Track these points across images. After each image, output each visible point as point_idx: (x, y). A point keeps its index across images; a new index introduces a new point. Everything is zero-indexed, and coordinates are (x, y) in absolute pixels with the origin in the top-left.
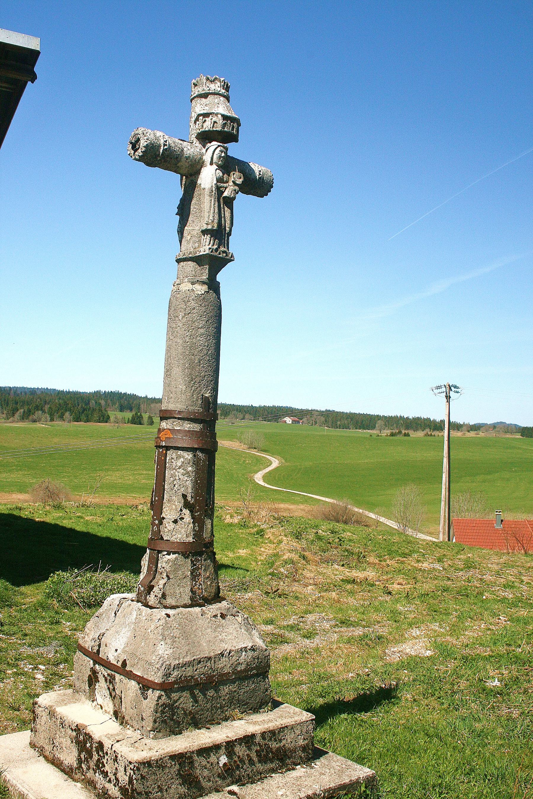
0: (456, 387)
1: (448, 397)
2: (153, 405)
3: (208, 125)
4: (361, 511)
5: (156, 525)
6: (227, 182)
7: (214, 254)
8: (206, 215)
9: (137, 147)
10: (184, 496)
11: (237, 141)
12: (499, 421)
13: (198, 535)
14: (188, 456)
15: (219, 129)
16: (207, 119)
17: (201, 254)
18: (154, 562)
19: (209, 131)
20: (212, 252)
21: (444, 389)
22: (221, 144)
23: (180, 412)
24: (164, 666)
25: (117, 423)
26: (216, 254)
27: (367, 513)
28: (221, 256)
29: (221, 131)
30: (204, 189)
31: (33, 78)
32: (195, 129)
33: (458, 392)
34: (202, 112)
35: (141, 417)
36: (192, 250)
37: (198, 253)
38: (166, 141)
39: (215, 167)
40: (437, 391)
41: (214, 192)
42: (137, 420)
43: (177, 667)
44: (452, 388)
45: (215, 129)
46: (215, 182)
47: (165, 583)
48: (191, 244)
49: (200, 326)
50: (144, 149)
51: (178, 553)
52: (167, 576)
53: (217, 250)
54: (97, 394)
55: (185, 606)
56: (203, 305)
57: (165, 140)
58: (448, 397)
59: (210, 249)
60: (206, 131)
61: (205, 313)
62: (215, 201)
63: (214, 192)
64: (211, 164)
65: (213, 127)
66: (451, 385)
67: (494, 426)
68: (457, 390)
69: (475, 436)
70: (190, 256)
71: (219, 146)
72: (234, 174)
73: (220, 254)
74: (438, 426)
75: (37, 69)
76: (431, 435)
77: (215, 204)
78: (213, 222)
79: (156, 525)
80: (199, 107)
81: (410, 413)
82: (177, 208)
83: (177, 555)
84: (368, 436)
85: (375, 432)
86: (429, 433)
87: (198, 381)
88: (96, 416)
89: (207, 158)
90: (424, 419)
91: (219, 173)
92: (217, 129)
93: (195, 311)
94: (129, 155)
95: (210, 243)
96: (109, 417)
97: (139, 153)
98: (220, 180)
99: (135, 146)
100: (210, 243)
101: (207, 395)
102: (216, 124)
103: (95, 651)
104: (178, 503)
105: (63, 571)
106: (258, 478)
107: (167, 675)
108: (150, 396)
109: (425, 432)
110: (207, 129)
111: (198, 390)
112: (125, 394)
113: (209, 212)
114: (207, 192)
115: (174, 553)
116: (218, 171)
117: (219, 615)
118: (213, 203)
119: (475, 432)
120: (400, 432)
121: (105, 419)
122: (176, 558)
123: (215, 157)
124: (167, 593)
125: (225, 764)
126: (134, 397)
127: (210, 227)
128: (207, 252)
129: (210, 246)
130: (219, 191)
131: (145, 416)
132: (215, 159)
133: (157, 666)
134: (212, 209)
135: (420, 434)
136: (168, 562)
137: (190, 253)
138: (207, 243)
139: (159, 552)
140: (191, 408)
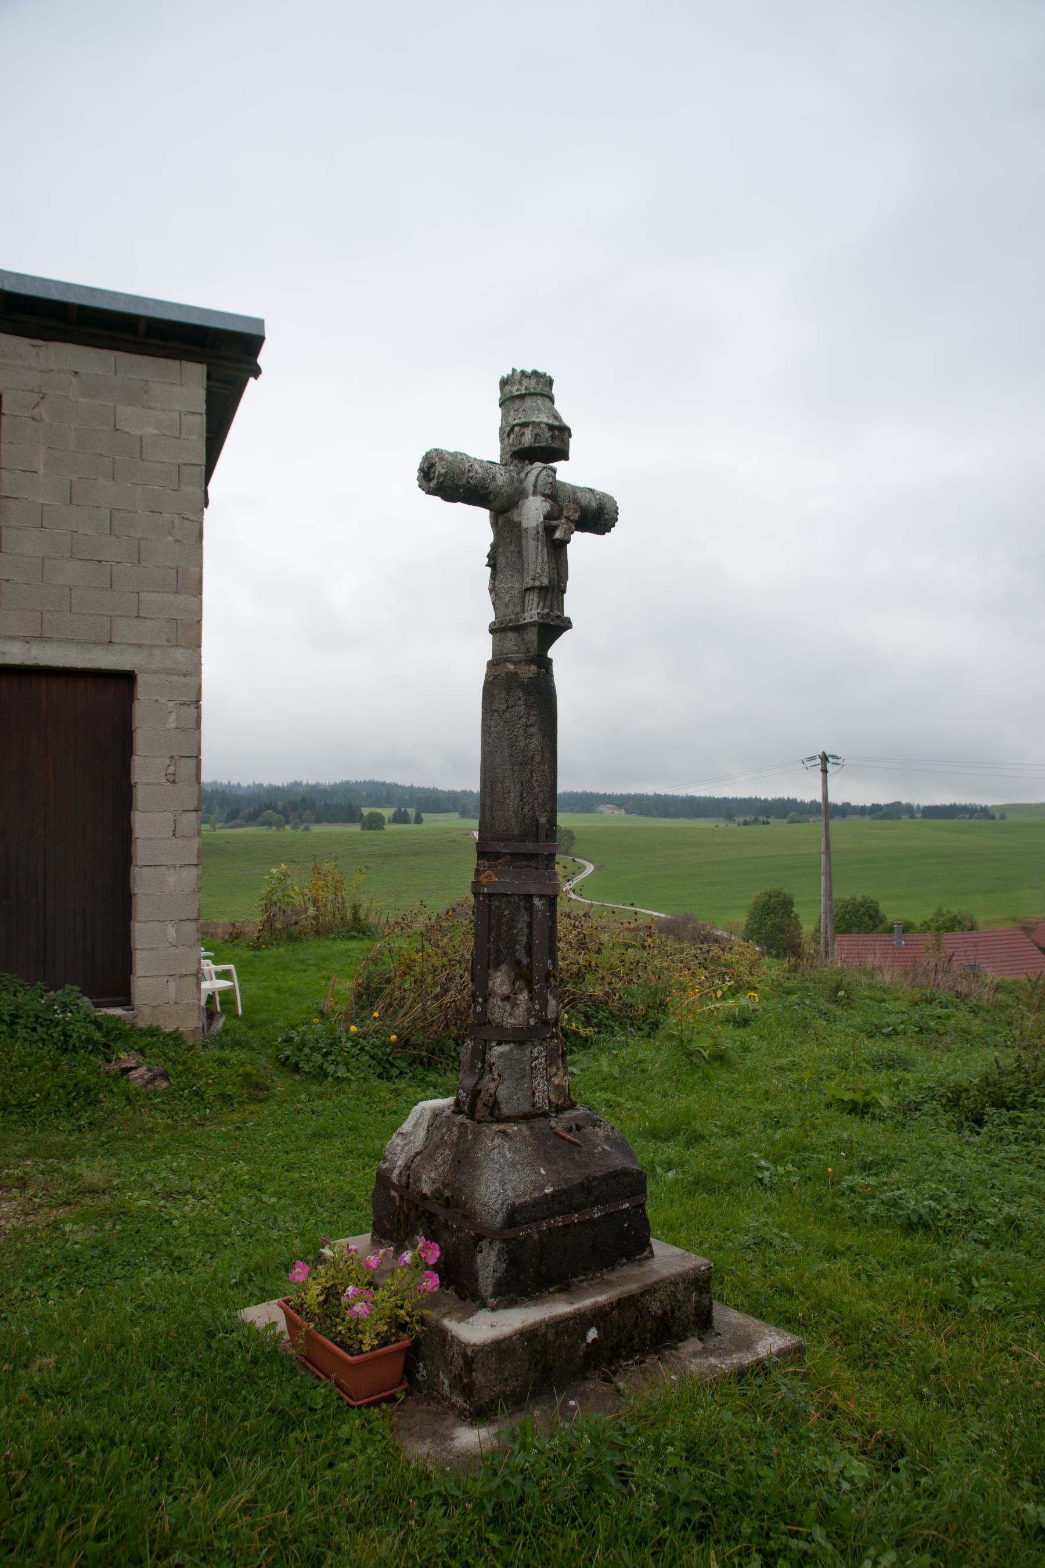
0: (834, 757)
1: (825, 771)
3: (528, 439)
5: (480, 1004)
7: (545, 621)
9: (432, 475)
11: (566, 458)
12: (488, 549)
17: (526, 621)
21: (819, 761)
30: (526, 530)
31: (256, 372)
33: (838, 764)
34: (517, 421)
36: (513, 616)
37: (521, 620)
40: (809, 764)
41: (541, 533)
44: (830, 759)
45: (537, 445)
48: (511, 608)
51: (514, 1042)
58: (825, 771)
62: (542, 547)
63: (541, 533)
65: (535, 442)
66: (827, 754)
68: (835, 761)
70: (511, 624)
71: (544, 468)
75: (262, 360)
77: (542, 551)
79: (480, 1004)
82: (488, 557)
83: (512, 1045)
92: (541, 445)
95: (538, 606)
103: (403, 1183)
114: (532, 533)
115: (507, 1042)
117: (574, 1128)
118: (540, 549)
120: (756, 820)
122: (511, 1050)
125: (594, 1340)
128: (536, 618)
129: (539, 611)
136: (501, 1055)
137: (511, 621)
138: (535, 606)
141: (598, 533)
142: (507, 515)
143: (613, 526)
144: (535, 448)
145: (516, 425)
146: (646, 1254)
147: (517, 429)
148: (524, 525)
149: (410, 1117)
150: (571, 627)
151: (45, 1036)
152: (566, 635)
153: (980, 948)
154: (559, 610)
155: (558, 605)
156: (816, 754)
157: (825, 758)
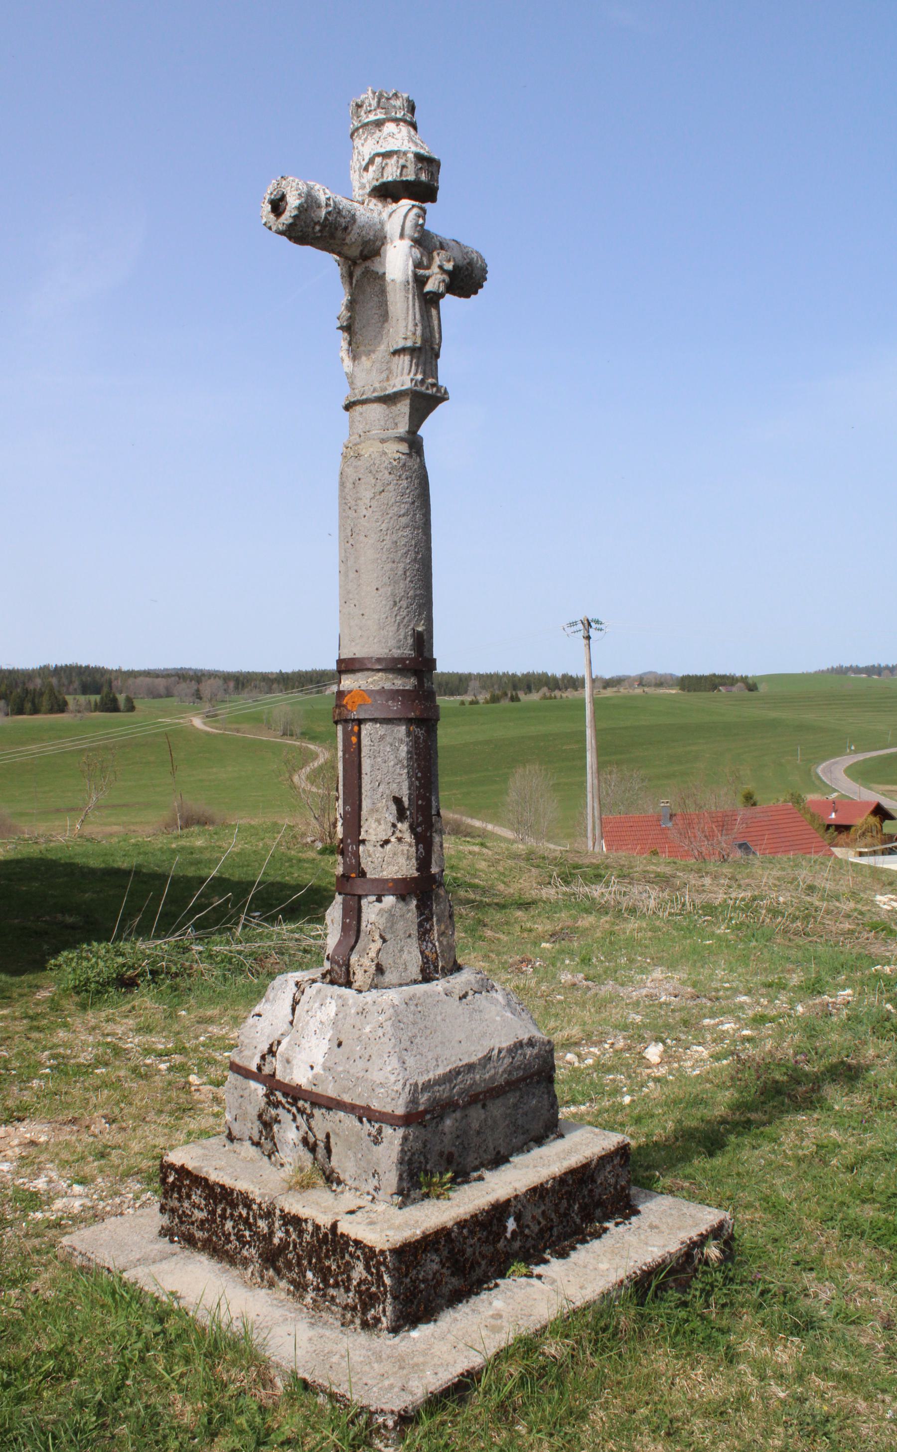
0: (597, 622)
2: (131, 681)
3: (392, 173)
4: (456, 816)
6: (428, 267)
7: (418, 388)
8: (402, 324)
10: (397, 801)
13: (424, 863)
14: (403, 728)
15: (411, 177)
16: (388, 161)
18: (353, 914)
19: (394, 183)
20: (416, 385)
21: (580, 626)
22: (417, 203)
23: (379, 660)
24: (408, 1086)
25: (79, 712)
26: (423, 389)
27: (469, 821)
28: (430, 392)
29: (414, 181)
32: (370, 178)
33: (601, 630)
35: (115, 700)
38: (328, 199)
39: (407, 243)
40: (570, 630)
42: (111, 705)
43: (428, 1086)
44: (593, 624)
45: (404, 179)
46: (411, 267)
47: (380, 950)
49: (402, 513)
50: (295, 213)
52: (382, 937)
53: (423, 381)
54: (44, 672)
55: (415, 982)
56: (404, 477)
57: (327, 196)
59: (412, 380)
60: (389, 183)
61: (408, 491)
62: (414, 298)
64: (402, 236)
65: (401, 174)
66: (590, 619)
67: (641, 681)
68: (599, 626)
69: (615, 694)
72: (438, 254)
73: (427, 388)
74: (574, 683)
76: (551, 698)
78: (414, 334)
80: (367, 146)
81: (519, 667)
84: (457, 705)
85: (468, 698)
86: (548, 694)
87: (405, 606)
88: (45, 702)
89: (392, 228)
90: (539, 675)
91: (417, 253)
93: (391, 487)
94: (265, 224)
95: (410, 371)
96: (65, 703)
97: (287, 217)
98: (418, 265)
99: (277, 206)
100: (410, 371)
101: (420, 629)
102: (405, 170)
104: (391, 813)
105: (99, 941)
106: (300, 779)
107: (414, 1101)
108: (125, 668)
109: (540, 694)
110: (390, 179)
111: (405, 621)
112: (87, 667)
113: (406, 319)
114: (399, 286)
116: (413, 249)
119: (615, 689)
121: (61, 707)
123: (409, 224)
124: (384, 963)
126: (101, 671)
127: (409, 344)
128: (408, 385)
130: (420, 281)
131: (121, 698)
132: (408, 230)
133: (395, 1088)
134: (411, 312)
135: (535, 697)
138: (406, 371)
139: (360, 897)
140: (396, 653)
141: (460, 296)
142: (368, 263)
143: (482, 286)
144: (402, 182)
145: (378, 155)
146: (492, 1285)
147: (378, 160)
148: (389, 277)
149: (557, 1168)
150: (447, 399)
151: (755, 1239)
152: (441, 407)
153: (752, 829)
154: (433, 378)
155: (431, 369)
156: (578, 619)
157: (588, 624)
